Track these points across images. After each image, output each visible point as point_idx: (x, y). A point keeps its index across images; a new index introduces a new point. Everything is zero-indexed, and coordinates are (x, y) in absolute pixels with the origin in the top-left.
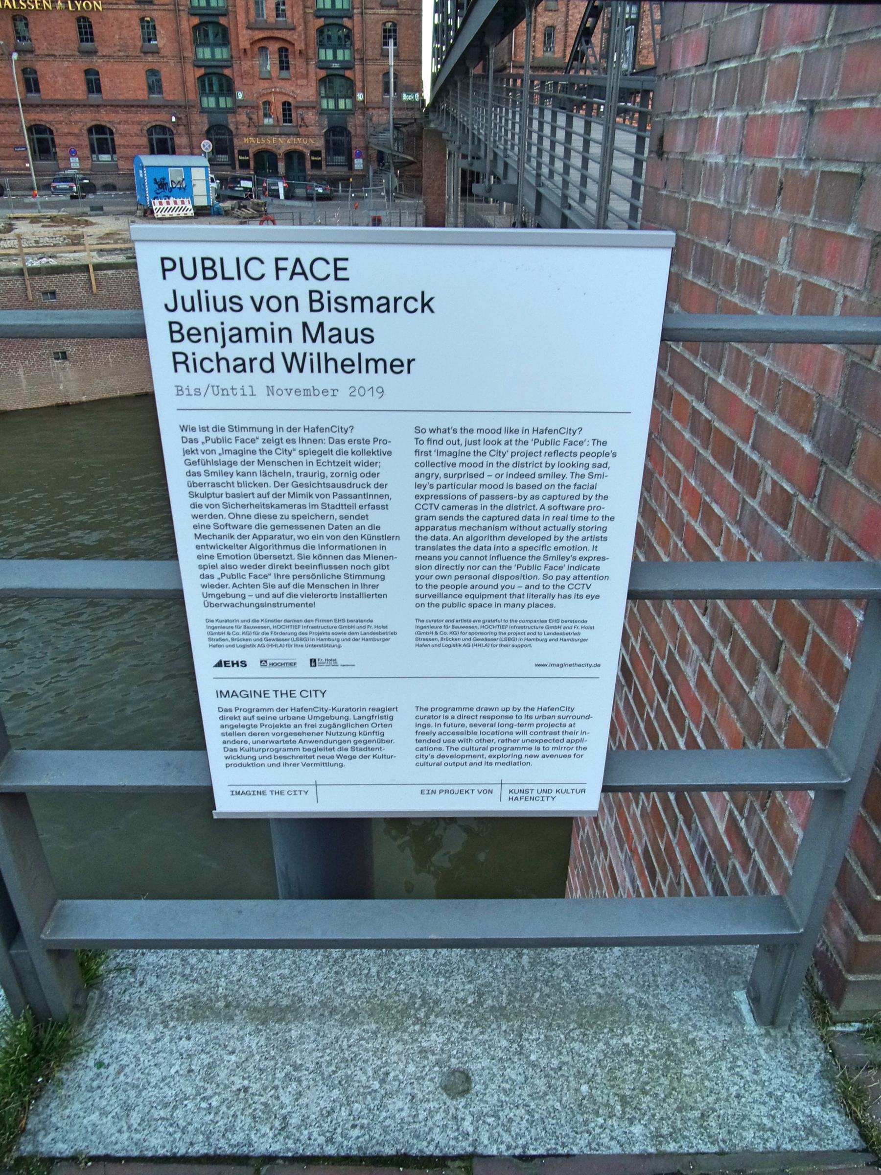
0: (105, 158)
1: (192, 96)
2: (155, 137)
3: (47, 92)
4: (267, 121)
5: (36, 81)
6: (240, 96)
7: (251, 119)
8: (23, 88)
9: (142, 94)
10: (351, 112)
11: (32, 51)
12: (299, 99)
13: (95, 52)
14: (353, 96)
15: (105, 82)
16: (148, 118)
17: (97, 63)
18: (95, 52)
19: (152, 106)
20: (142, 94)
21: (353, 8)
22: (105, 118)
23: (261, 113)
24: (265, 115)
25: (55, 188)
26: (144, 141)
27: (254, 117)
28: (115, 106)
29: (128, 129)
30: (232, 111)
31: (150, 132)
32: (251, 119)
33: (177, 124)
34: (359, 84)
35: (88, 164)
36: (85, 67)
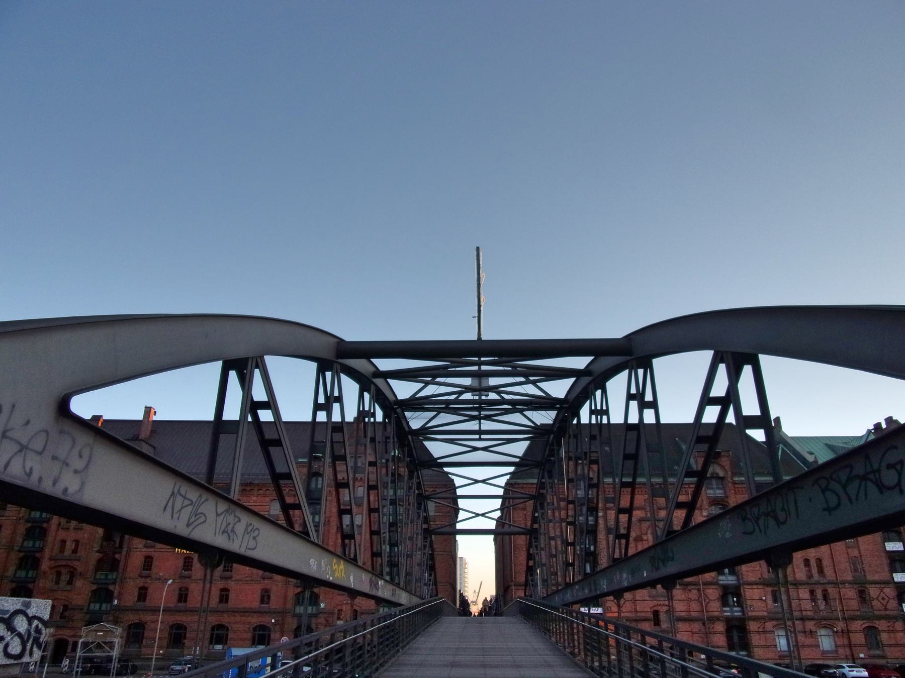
0: (219, 647)
1: (289, 606)
2: (215, 632)
3: (234, 601)
4: (340, 623)
5: (186, 595)
6: (323, 605)
7: (327, 621)
8: (218, 600)
9: (256, 604)
10: (316, 616)
11: (190, 577)
12: (363, 608)
13: (230, 578)
14: (111, 601)
15: (232, 596)
16: (255, 620)
17: (231, 584)
18: (190, 577)
19: (260, 612)
20: (256, 604)
21: (716, 583)
22: (225, 620)
23: (336, 616)
24: (339, 619)
25: (172, 670)
26: (249, 635)
27: (330, 620)
28: (235, 612)
29: (240, 626)
30: (316, 616)
31: (255, 629)
32: (327, 621)
33: (275, 624)
34: (116, 594)
35: (205, 651)
36: (141, 585)
